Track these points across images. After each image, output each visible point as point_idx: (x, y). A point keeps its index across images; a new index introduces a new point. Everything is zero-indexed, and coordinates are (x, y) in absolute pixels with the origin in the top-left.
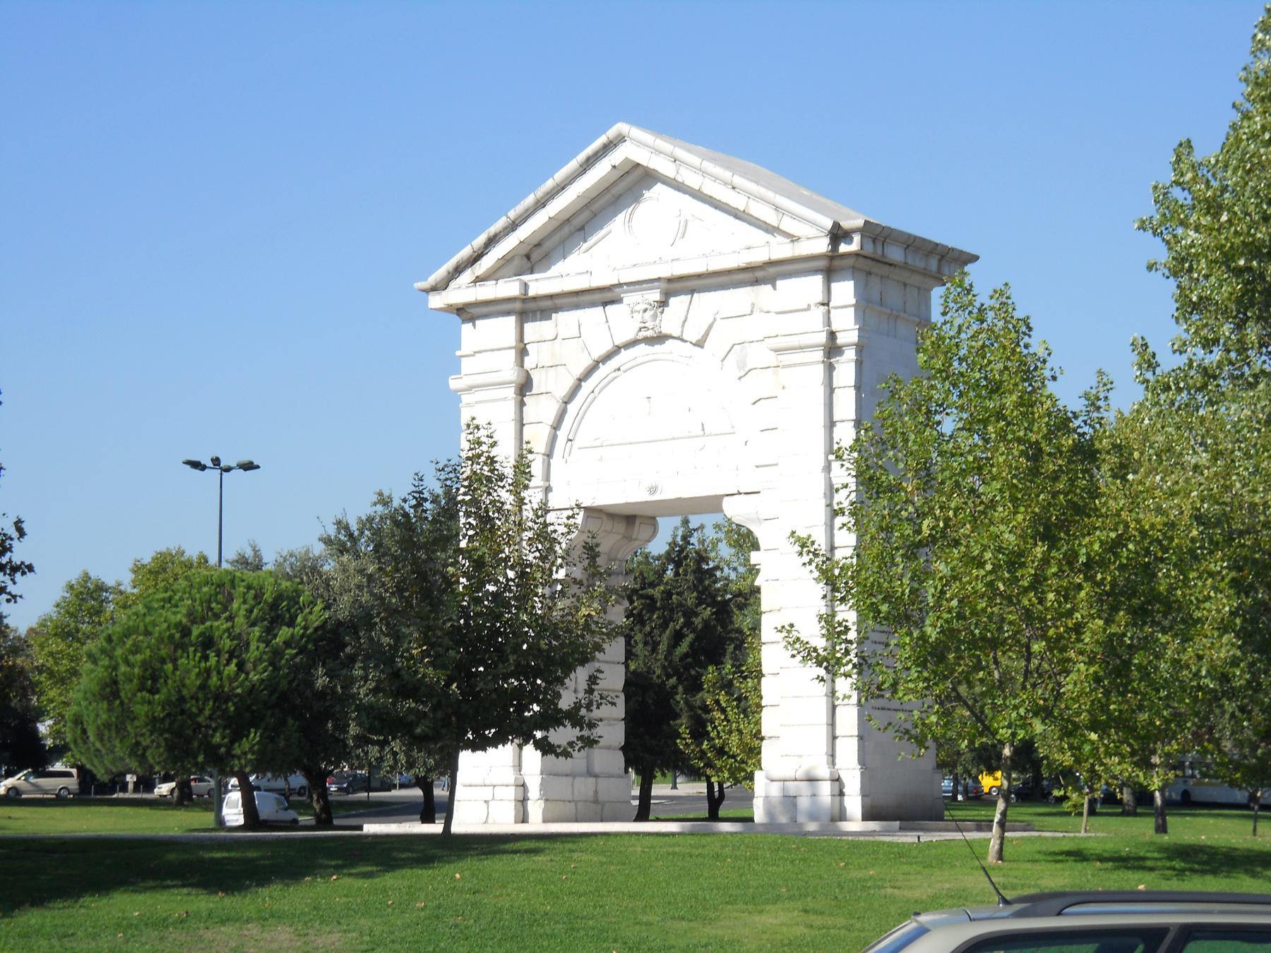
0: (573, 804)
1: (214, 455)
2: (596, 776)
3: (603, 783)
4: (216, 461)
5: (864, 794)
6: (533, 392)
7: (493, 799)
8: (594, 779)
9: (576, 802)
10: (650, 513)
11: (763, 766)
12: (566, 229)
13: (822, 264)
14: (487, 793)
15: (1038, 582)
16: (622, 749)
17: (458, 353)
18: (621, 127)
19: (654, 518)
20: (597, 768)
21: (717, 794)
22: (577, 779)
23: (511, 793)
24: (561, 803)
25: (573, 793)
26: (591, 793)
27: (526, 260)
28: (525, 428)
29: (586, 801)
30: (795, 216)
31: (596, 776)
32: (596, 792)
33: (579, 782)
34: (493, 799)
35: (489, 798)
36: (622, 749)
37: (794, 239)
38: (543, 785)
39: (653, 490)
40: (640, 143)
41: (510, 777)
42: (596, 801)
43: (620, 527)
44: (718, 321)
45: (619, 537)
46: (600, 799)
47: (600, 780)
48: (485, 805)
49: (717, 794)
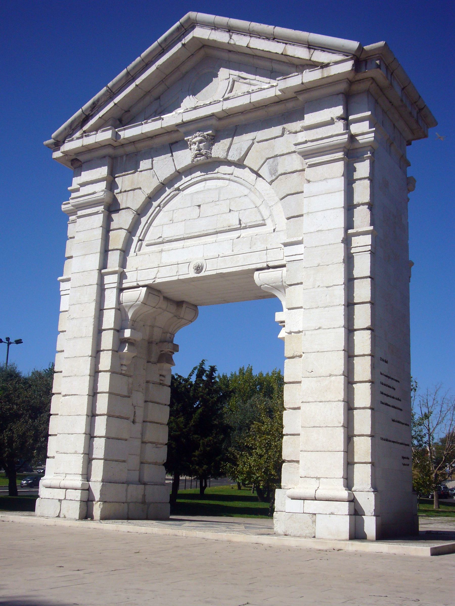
0: (126, 504)
1: (8, 337)
2: (145, 484)
4: (8, 339)
5: (377, 514)
7: (65, 499)
8: (143, 486)
9: (128, 503)
10: (195, 303)
12: (148, 99)
13: (342, 87)
14: (60, 494)
15: (254, 431)
16: (164, 465)
17: (69, 188)
18: (192, 14)
19: (196, 306)
20: (146, 479)
21: (204, 485)
23: (77, 495)
25: (126, 497)
26: (140, 497)
27: (118, 122)
28: (111, 233)
31: (145, 484)
32: (144, 495)
33: (132, 488)
34: (65, 499)
38: (102, 492)
39: (199, 269)
40: (205, 24)
41: (78, 482)
42: (144, 502)
43: (173, 308)
44: (256, 144)
45: (171, 315)
47: (147, 487)
48: (59, 503)
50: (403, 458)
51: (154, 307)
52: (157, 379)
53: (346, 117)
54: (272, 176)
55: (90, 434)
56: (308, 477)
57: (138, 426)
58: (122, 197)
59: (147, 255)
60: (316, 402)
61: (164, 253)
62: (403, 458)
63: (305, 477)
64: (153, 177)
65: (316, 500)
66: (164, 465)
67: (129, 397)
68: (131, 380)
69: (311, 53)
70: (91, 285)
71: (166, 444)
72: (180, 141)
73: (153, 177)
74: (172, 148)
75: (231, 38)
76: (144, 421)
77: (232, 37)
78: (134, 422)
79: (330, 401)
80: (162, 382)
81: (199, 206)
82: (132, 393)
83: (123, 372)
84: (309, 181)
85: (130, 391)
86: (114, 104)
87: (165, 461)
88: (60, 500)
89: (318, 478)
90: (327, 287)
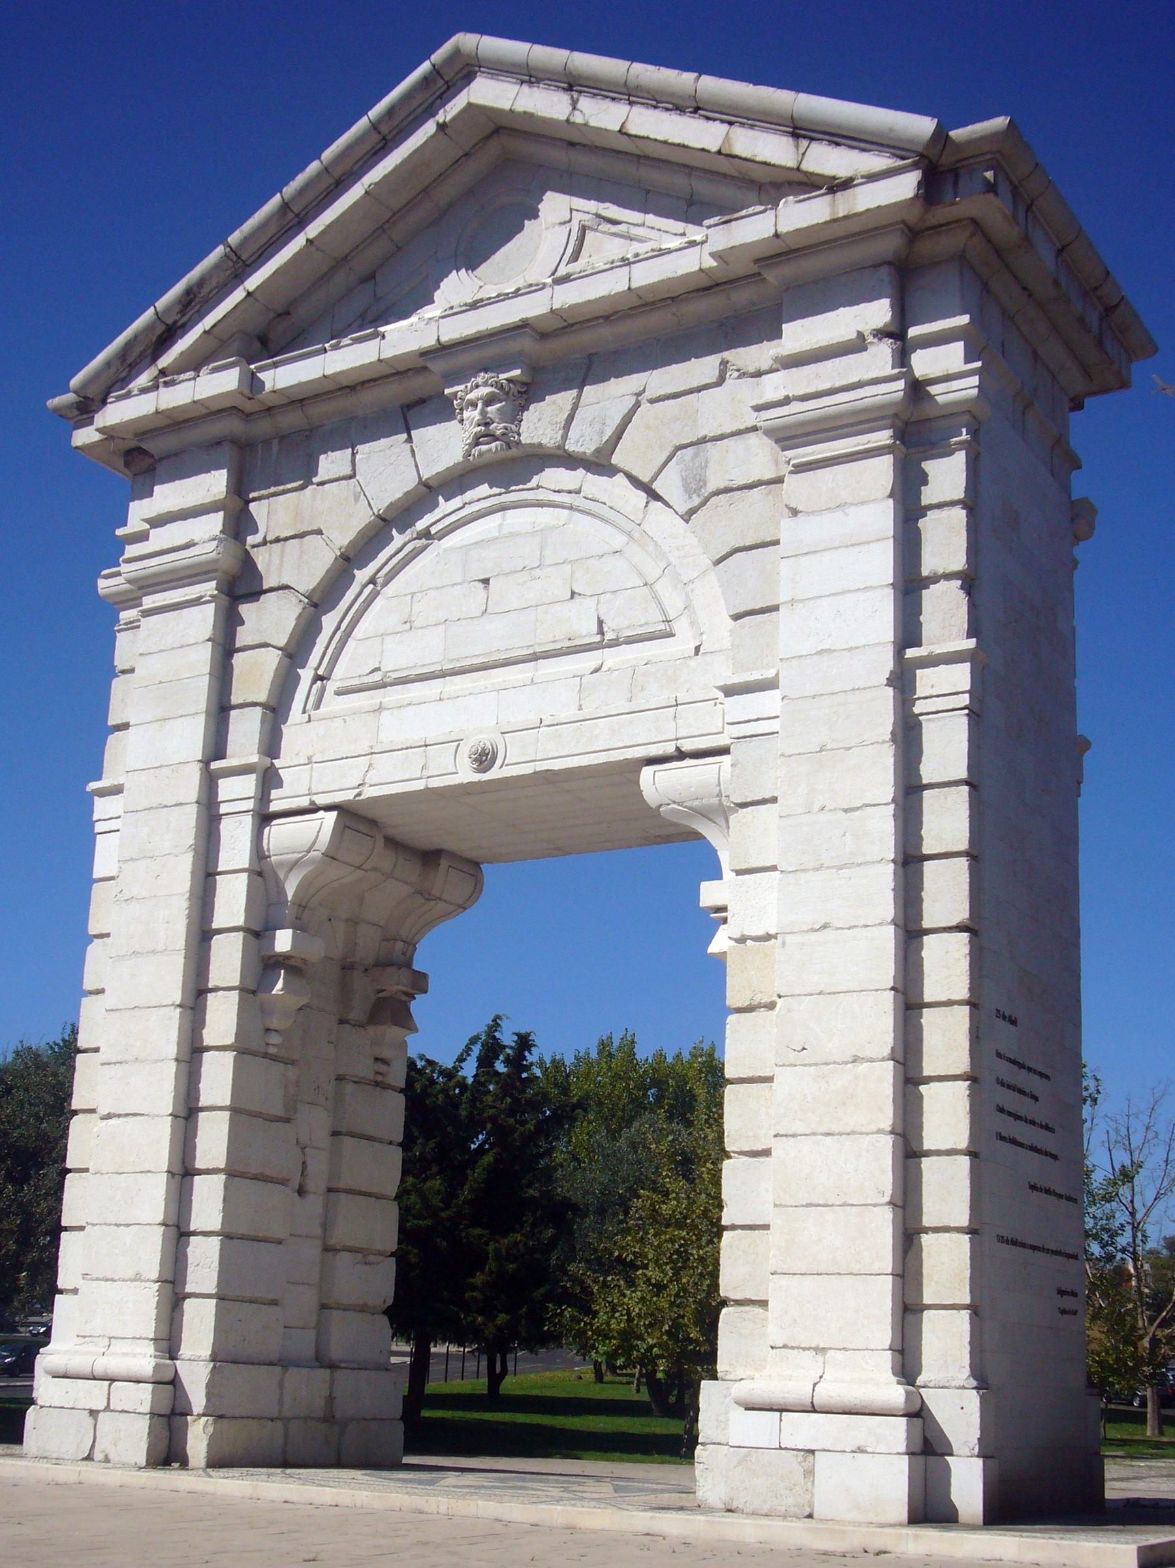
0: (279, 1424)
2: (332, 1366)
3: (345, 1378)
6: (288, 723)
7: (107, 1408)
8: (328, 1372)
10: (473, 854)
11: (720, 1367)
12: (341, 280)
13: (890, 245)
14: (93, 1394)
16: (388, 1312)
17: (120, 532)
18: (466, 41)
19: (476, 865)
20: (336, 1351)
21: (498, 1370)
22: (293, 1372)
24: (254, 1423)
25: (281, 1402)
26: (320, 1402)
28: (238, 659)
29: (306, 1418)
30: (837, 136)
31: (332, 1366)
32: (331, 1399)
33: (295, 1376)
35: (101, 1405)
36: (401, 1419)
37: (837, 186)
39: (484, 759)
40: (502, 69)
42: (329, 1418)
43: (411, 870)
46: (338, 1415)
47: (339, 1374)
48: (90, 1421)
49: (498, 1370)
50: (1061, 1292)
51: (358, 868)
52: (365, 1069)
53: (898, 332)
54: (690, 497)
55: (178, 1227)
56: (793, 1348)
57: (314, 1204)
58: (267, 556)
59: (340, 720)
60: (814, 1134)
61: (385, 713)
62: (1061, 1292)
63: (785, 1346)
64: (357, 499)
65: (815, 1411)
66: (388, 1312)
67: (288, 1120)
68: (292, 1072)
69: (802, 150)
70: (181, 804)
71: (392, 1254)
72: (431, 398)
73: (357, 499)
74: (409, 417)
75: (574, 108)
76: (330, 1190)
77: (579, 106)
78: (301, 1191)
79: (853, 1133)
80: (380, 1078)
81: (486, 582)
82: (295, 1111)
83: (272, 1050)
84: (795, 512)
85: (291, 1105)
86: (244, 294)
87: (390, 1302)
88: (93, 1413)
89: (820, 1350)
90: (846, 811)
